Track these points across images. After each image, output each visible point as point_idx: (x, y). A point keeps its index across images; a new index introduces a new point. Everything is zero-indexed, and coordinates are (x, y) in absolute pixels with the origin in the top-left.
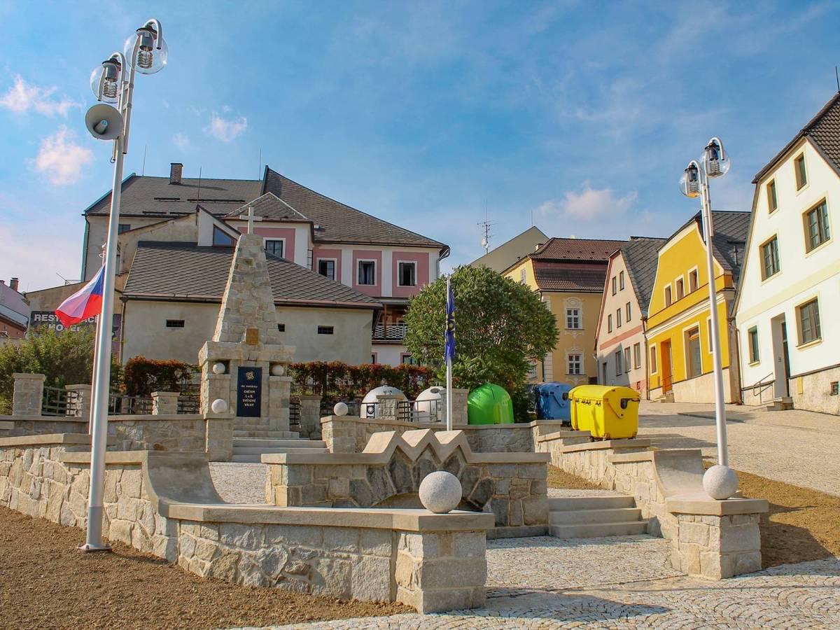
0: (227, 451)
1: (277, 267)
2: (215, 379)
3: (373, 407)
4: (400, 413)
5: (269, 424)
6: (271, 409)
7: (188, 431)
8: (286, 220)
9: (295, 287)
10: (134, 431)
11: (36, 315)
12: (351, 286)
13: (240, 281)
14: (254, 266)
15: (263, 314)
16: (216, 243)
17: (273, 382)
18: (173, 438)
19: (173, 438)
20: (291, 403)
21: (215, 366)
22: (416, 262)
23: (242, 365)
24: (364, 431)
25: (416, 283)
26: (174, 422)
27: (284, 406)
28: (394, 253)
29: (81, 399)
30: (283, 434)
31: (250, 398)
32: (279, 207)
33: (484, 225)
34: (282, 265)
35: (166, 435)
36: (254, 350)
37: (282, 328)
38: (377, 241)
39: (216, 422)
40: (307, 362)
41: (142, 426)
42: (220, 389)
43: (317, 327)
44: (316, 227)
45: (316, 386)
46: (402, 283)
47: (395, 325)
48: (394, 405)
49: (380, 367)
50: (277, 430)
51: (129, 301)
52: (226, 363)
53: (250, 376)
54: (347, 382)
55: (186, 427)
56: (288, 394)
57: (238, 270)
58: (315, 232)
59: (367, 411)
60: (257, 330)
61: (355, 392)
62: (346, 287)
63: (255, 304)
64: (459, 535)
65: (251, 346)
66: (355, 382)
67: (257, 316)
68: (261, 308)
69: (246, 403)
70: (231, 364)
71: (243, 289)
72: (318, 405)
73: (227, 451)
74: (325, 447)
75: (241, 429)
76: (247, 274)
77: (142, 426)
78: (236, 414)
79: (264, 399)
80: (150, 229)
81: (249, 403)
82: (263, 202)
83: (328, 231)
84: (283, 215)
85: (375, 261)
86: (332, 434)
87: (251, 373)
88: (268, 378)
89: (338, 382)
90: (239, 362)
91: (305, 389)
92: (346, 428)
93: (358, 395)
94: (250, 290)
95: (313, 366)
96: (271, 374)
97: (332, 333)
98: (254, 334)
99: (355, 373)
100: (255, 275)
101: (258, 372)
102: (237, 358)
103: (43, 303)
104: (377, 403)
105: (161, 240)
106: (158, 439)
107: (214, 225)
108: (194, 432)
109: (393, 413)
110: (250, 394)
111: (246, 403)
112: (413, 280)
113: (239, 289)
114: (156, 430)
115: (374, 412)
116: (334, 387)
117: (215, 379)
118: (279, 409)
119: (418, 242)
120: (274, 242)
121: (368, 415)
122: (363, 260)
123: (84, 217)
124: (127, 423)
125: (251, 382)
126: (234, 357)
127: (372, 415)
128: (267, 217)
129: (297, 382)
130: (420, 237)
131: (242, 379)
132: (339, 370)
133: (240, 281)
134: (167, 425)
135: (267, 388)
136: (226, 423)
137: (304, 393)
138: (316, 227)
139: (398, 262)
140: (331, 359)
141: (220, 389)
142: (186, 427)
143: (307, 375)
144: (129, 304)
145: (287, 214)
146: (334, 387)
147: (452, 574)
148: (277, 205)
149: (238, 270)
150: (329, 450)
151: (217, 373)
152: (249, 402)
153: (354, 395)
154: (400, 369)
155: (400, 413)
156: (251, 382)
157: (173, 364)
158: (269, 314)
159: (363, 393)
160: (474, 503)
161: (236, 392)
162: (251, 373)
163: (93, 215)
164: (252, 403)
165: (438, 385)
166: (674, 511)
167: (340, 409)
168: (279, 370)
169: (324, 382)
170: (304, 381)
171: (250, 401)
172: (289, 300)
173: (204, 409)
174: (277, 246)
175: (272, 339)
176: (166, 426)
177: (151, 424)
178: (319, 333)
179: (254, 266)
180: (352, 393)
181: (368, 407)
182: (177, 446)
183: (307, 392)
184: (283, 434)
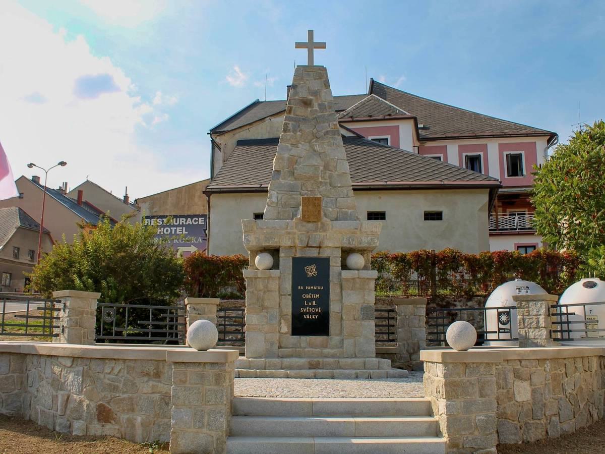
0: (213, 433)
1: (377, 153)
2: (256, 278)
3: (508, 313)
4: (553, 323)
5: (342, 347)
6: (345, 323)
7: (151, 383)
9: (396, 170)
10: (71, 376)
12: (457, 164)
13: (295, 131)
14: (316, 107)
15: (330, 177)
17: (347, 280)
18: (125, 396)
19: (125, 396)
20: (376, 310)
21: (258, 258)
22: (523, 153)
23: (298, 255)
24: (511, 376)
25: (524, 173)
26: (128, 363)
27: (366, 317)
29: (67, 311)
31: (312, 306)
32: (382, 106)
33: (578, 125)
34: (381, 151)
35: (115, 389)
36: (316, 230)
38: (482, 134)
39: (190, 369)
40: (407, 250)
41: (81, 368)
42: (265, 292)
44: (420, 126)
45: (422, 282)
46: (510, 174)
47: (506, 215)
48: (543, 311)
49: (240, 399)
50: (356, 357)
51: (213, 195)
52: (274, 252)
53: (311, 271)
54: (462, 276)
55: (148, 374)
56: (371, 298)
57: (292, 115)
58: (420, 131)
59: (499, 320)
60: (319, 199)
61: (474, 289)
62: (455, 167)
63: (317, 161)
65: (310, 225)
66: (474, 276)
67: (320, 180)
68: (326, 167)
69: (306, 313)
70: (282, 254)
71: (298, 142)
72: (423, 312)
73: (213, 433)
74: (430, 414)
75: (300, 356)
76: (305, 120)
77: (81, 368)
78: (290, 332)
79: (334, 308)
80: (248, 127)
81: (310, 314)
82: (367, 103)
83: (432, 129)
84: (387, 114)
85: (482, 154)
86: (442, 390)
87: (313, 267)
88: (340, 274)
89: (451, 275)
90: (294, 250)
91: (408, 287)
92: (473, 378)
93: (478, 293)
94: (310, 142)
95: (417, 256)
96: (344, 267)
98: (314, 205)
99: (474, 264)
100: (317, 120)
101: (323, 264)
102: (289, 243)
103: (151, 208)
104: (514, 308)
105: (259, 137)
106: (103, 394)
108: (160, 385)
109: (542, 323)
110: (311, 300)
112: (521, 170)
113: (293, 141)
114: (102, 376)
115: (508, 321)
116: (445, 283)
117: (256, 278)
118: (359, 322)
119: (524, 132)
121: (501, 326)
122: (469, 154)
124: (63, 361)
125: (312, 281)
126: (285, 242)
127: (507, 327)
128: (371, 116)
129: (397, 278)
130: (526, 127)
131: (299, 276)
132: (452, 261)
133: (295, 131)
134: (118, 367)
135: (338, 291)
136: (210, 372)
137: (405, 292)
138: (420, 126)
140: (439, 246)
141: (265, 292)
142: (148, 374)
143: (410, 267)
144: (213, 198)
146: (445, 283)
148: (380, 105)
149: (292, 115)
150: (437, 423)
151: (261, 268)
152: (310, 313)
153: (473, 293)
154: (534, 256)
155: (553, 323)
156: (312, 281)
157: (240, 261)
158: (339, 175)
159: (486, 290)
161: (290, 297)
162: (313, 267)
163: (217, 133)
164: (315, 313)
165: (592, 276)
167: (460, 335)
168: (357, 260)
169: (433, 276)
170: (406, 277)
171: (312, 310)
172: (388, 183)
173: (179, 338)
175: (346, 213)
176: (116, 371)
177: (93, 365)
179: (316, 107)
180: (471, 290)
181: (499, 314)
182: (133, 410)
183: (410, 291)
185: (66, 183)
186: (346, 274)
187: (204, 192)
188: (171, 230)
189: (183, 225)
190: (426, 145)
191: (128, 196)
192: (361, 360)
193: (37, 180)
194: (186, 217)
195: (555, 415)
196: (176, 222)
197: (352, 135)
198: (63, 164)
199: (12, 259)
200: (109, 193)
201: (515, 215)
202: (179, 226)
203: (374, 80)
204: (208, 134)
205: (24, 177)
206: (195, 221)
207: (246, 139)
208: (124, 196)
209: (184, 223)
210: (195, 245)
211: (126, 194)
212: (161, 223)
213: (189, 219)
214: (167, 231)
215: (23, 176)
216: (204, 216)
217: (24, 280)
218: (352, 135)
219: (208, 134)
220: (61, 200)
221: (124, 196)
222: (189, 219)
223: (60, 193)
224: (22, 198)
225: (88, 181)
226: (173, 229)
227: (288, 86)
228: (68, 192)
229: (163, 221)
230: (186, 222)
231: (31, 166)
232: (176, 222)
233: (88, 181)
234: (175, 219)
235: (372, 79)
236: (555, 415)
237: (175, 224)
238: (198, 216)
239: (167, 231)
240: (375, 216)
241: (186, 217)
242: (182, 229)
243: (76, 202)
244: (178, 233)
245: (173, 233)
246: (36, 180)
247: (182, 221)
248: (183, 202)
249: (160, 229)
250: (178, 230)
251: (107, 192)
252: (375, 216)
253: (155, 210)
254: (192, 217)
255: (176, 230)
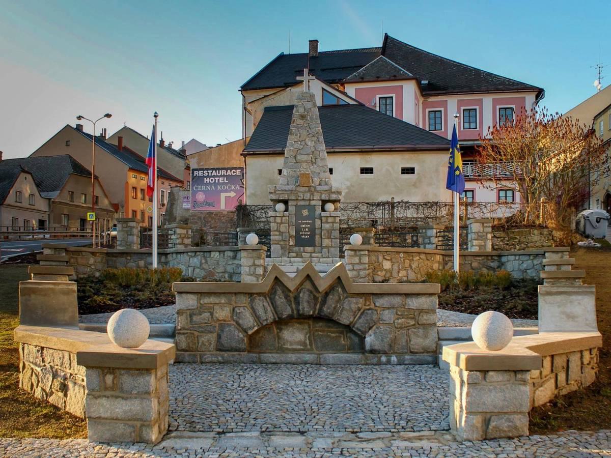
8: (395, 78)
11: (195, 172)
16: (325, 104)
28: (493, 99)
30: (290, 261)
31: (306, 231)
37: (280, 172)
43: (359, 169)
52: (285, 202)
64: (123, 372)
69: (303, 235)
80: (273, 96)
96: (323, 210)
97: (414, 173)
98: (306, 177)
107: (323, 88)
111: (303, 235)
120: (386, 98)
123: (240, 92)
139: (498, 107)
145: (395, 74)
147: (117, 408)
160: (357, 331)
164: (308, 235)
166: (528, 346)
174: (388, 101)
178: (362, 173)
184: (290, 261)
185: (105, 129)
186: (323, 214)
187: (241, 155)
188: (215, 180)
189: (224, 176)
190: (429, 100)
191: (164, 140)
192: (331, 259)
193: (80, 128)
194: (227, 169)
195: (405, 276)
196: (219, 173)
197: (355, 103)
198: (108, 116)
199: (68, 202)
200: (145, 138)
201: (468, 164)
202: (221, 176)
203: (389, 34)
204: (239, 91)
205: (69, 126)
206: (234, 172)
207: (272, 106)
208: (160, 141)
209: (225, 174)
210: (234, 191)
211: (162, 139)
212: (207, 174)
213: (229, 171)
214: (212, 180)
215: (68, 125)
216: (242, 169)
217: (79, 221)
218: (355, 103)
219: (239, 91)
220: (104, 147)
221: (160, 141)
222: (229, 171)
223: (100, 140)
224: (69, 145)
225: (125, 127)
226: (217, 179)
227: (310, 41)
228: (107, 138)
229: (208, 173)
230: (226, 173)
231: (79, 118)
232: (219, 173)
233: (125, 127)
234: (217, 171)
235: (386, 34)
236: (405, 276)
237: (218, 175)
238: (236, 168)
239: (212, 180)
240: (365, 171)
241: (227, 169)
242: (224, 179)
243: (117, 149)
244: (220, 182)
245: (217, 182)
246: (79, 128)
247: (223, 172)
248: (223, 158)
249: (207, 179)
250: (220, 180)
251: (144, 137)
252: (365, 171)
253: (202, 164)
254: (231, 169)
255: (219, 180)
